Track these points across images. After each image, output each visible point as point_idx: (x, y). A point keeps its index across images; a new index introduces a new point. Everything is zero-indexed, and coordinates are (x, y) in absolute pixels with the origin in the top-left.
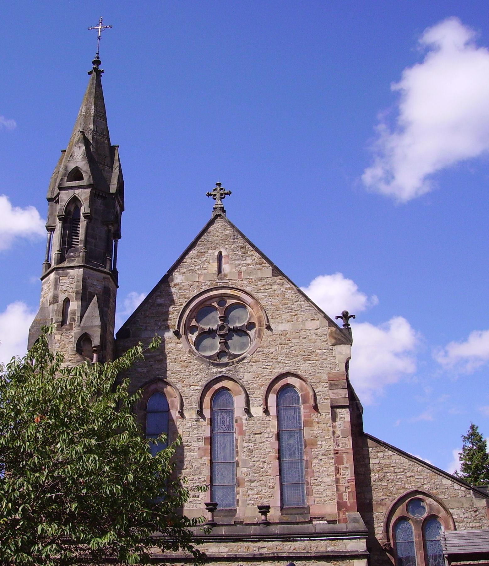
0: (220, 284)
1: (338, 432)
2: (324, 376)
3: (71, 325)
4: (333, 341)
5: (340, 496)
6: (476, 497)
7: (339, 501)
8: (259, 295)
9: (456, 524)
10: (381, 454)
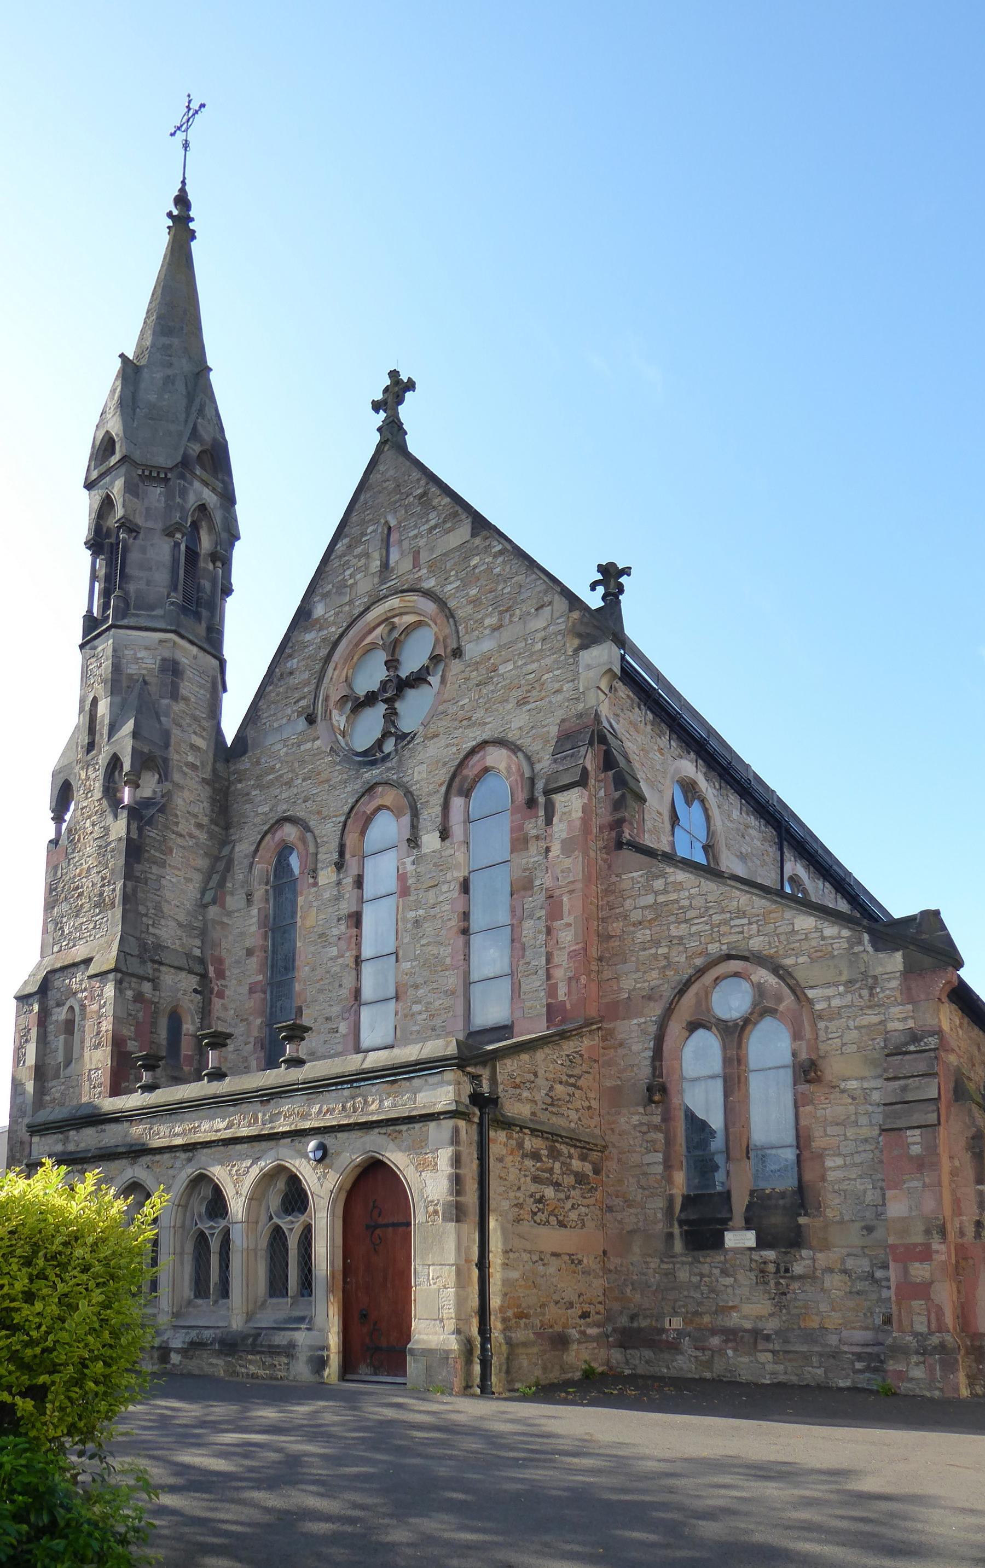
1: (556, 849)
2: (554, 731)
4: (577, 642)
5: (552, 991)
7: (550, 1001)
10: (658, 884)
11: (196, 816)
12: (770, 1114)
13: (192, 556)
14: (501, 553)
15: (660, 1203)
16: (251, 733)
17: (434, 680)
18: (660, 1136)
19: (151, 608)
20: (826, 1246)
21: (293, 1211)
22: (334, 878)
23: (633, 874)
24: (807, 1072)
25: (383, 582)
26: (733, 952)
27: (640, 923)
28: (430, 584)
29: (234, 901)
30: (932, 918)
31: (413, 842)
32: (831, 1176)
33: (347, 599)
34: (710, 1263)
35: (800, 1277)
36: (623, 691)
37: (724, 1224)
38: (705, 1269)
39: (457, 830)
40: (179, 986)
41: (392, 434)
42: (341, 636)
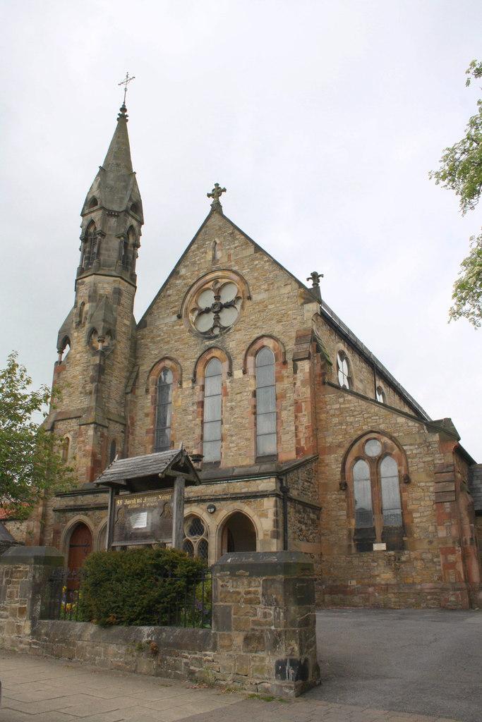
1: (299, 383)
2: (294, 335)
3: (84, 323)
4: (303, 301)
5: (298, 442)
9: (409, 460)
10: (341, 400)
11: (124, 354)
12: (391, 494)
13: (126, 245)
14: (268, 261)
15: (345, 532)
16: (149, 319)
17: (238, 306)
18: (345, 504)
19: (110, 266)
20: (414, 549)
21: (195, 534)
22: (191, 385)
23: (330, 396)
24: (406, 480)
25: (214, 264)
26: (374, 430)
27: (334, 415)
28: (235, 268)
29: (140, 391)
30: (448, 421)
31: (230, 374)
32: (416, 520)
33: (197, 269)
34: (366, 556)
35: (405, 562)
36: (320, 319)
37: (373, 541)
38: (365, 559)
39: (251, 371)
40: (115, 429)
41: (217, 208)
42: (194, 283)
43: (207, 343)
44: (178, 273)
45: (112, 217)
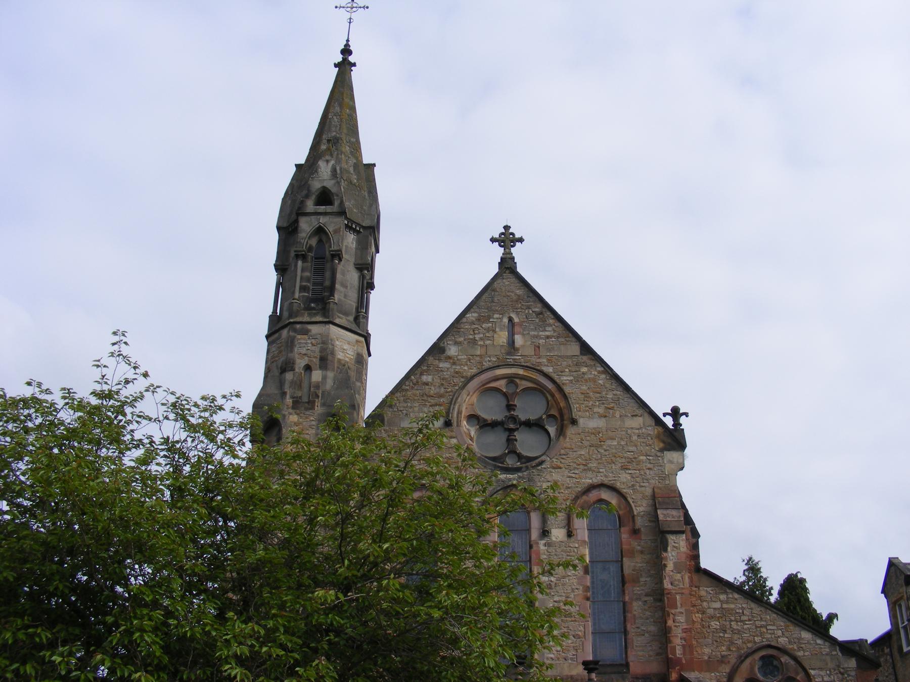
0: (510, 361)
4: (662, 445)
6: (843, 655)
8: (565, 379)
41: (507, 265)
43: (502, 476)
44: (443, 350)
45: (326, 229)
